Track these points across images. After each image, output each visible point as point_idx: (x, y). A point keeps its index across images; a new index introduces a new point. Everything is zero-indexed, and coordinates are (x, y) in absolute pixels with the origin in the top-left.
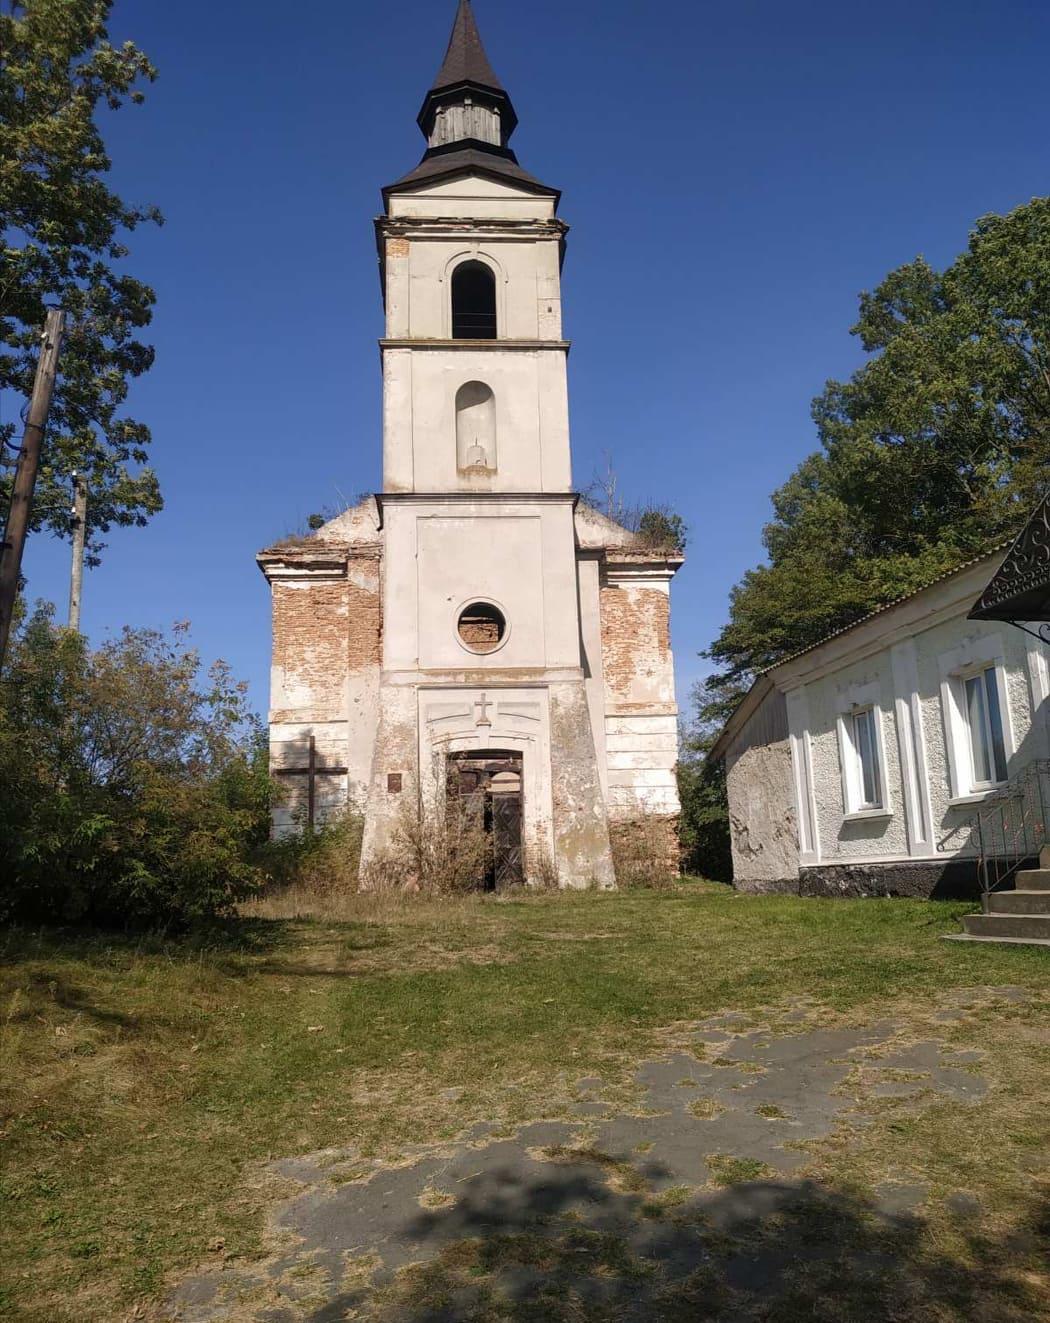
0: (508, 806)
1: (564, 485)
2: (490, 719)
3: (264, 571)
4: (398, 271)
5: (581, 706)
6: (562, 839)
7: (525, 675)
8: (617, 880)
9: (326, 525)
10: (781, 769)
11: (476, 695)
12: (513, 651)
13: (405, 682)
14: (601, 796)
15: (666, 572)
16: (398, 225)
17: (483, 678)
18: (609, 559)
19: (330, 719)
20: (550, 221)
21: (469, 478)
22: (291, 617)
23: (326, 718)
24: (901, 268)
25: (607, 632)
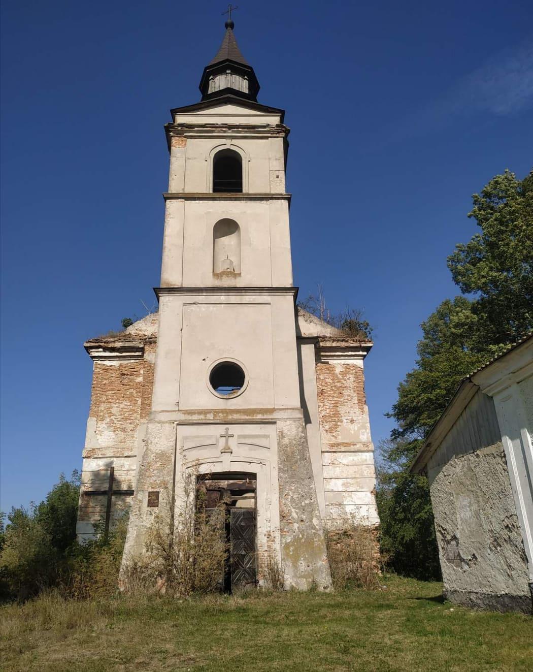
0: (243, 519)
1: (288, 282)
2: (231, 448)
3: (89, 354)
4: (178, 155)
5: (301, 437)
6: (287, 546)
7: (259, 413)
8: (333, 582)
9: (133, 324)
10: (494, 473)
11: (221, 429)
12: (249, 397)
13: (166, 420)
14: (318, 510)
15: (361, 353)
16: (180, 128)
17: (227, 416)
18: (322, 344)
19: (126, 454)
20: (277, 126)
21: (221, 279)
22: (105, 384)
23: (123, 454)
24: (474, 237)
25: (321, 393)
